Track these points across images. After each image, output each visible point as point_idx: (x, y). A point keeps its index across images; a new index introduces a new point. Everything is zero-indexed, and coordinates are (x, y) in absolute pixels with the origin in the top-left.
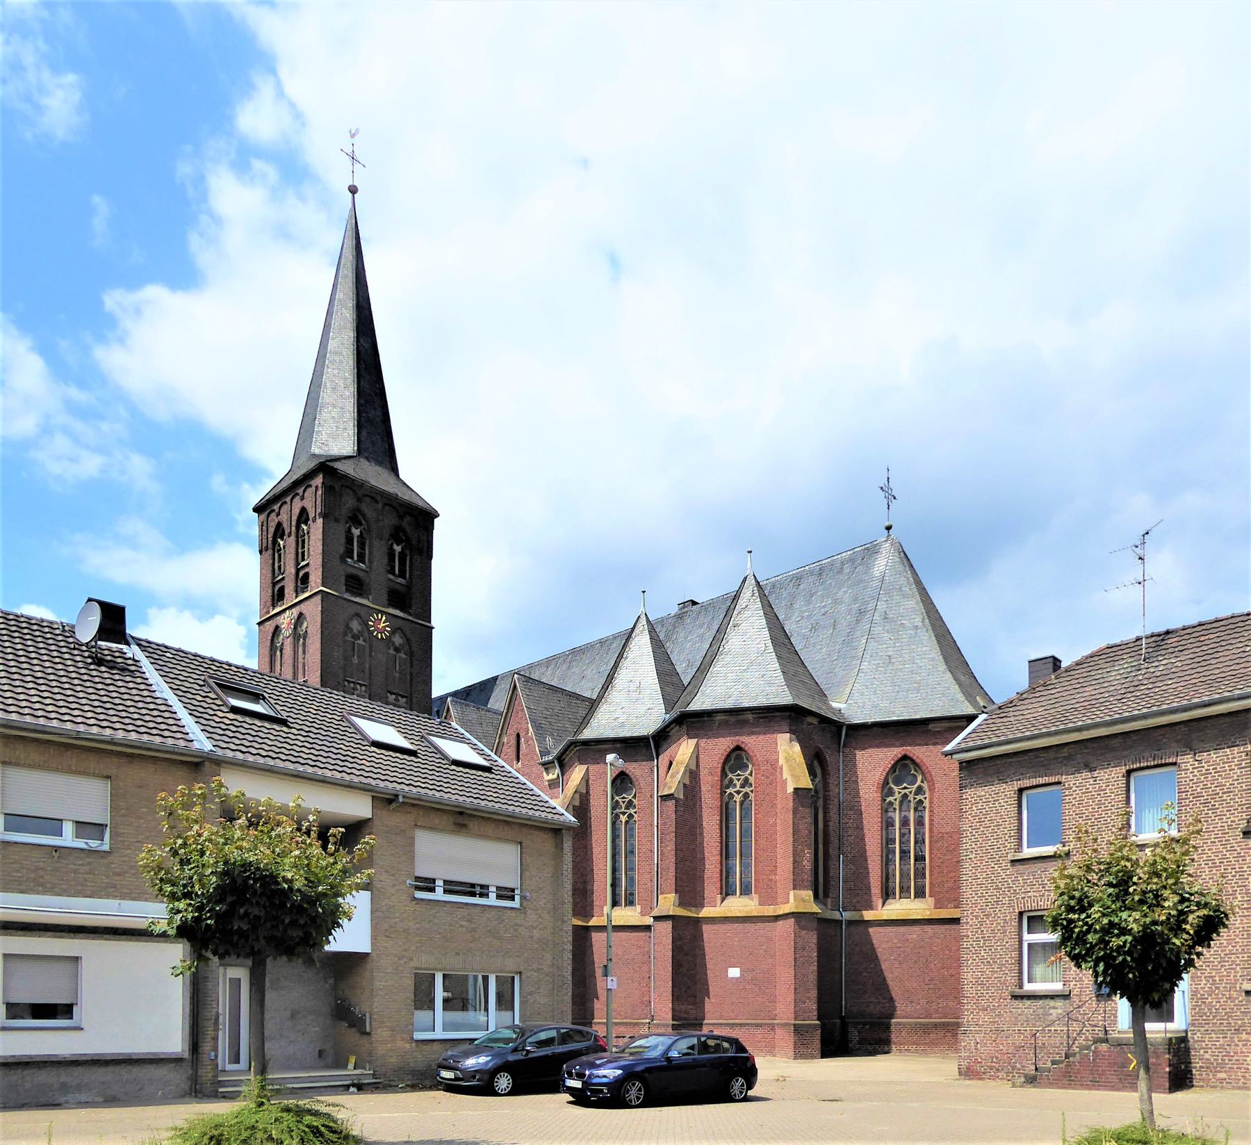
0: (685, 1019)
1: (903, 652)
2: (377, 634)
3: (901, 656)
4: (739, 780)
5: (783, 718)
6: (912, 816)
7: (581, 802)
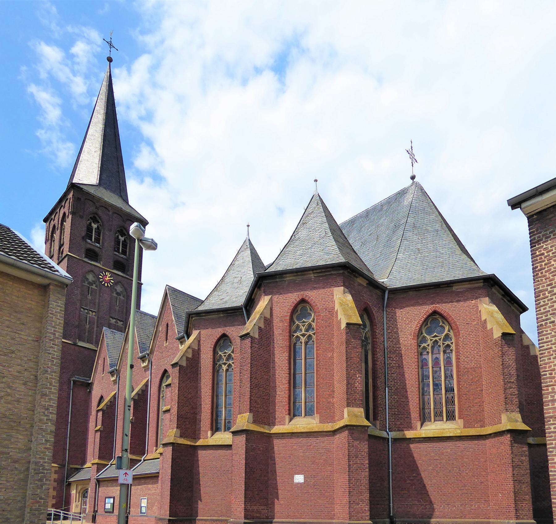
0: (257, 517)
1: (428, 246)
2: (105, 283)
3: (427, 248)
4: (304, 326)
5: (339, 275)
6: (442, 357)
7: (193, 355)
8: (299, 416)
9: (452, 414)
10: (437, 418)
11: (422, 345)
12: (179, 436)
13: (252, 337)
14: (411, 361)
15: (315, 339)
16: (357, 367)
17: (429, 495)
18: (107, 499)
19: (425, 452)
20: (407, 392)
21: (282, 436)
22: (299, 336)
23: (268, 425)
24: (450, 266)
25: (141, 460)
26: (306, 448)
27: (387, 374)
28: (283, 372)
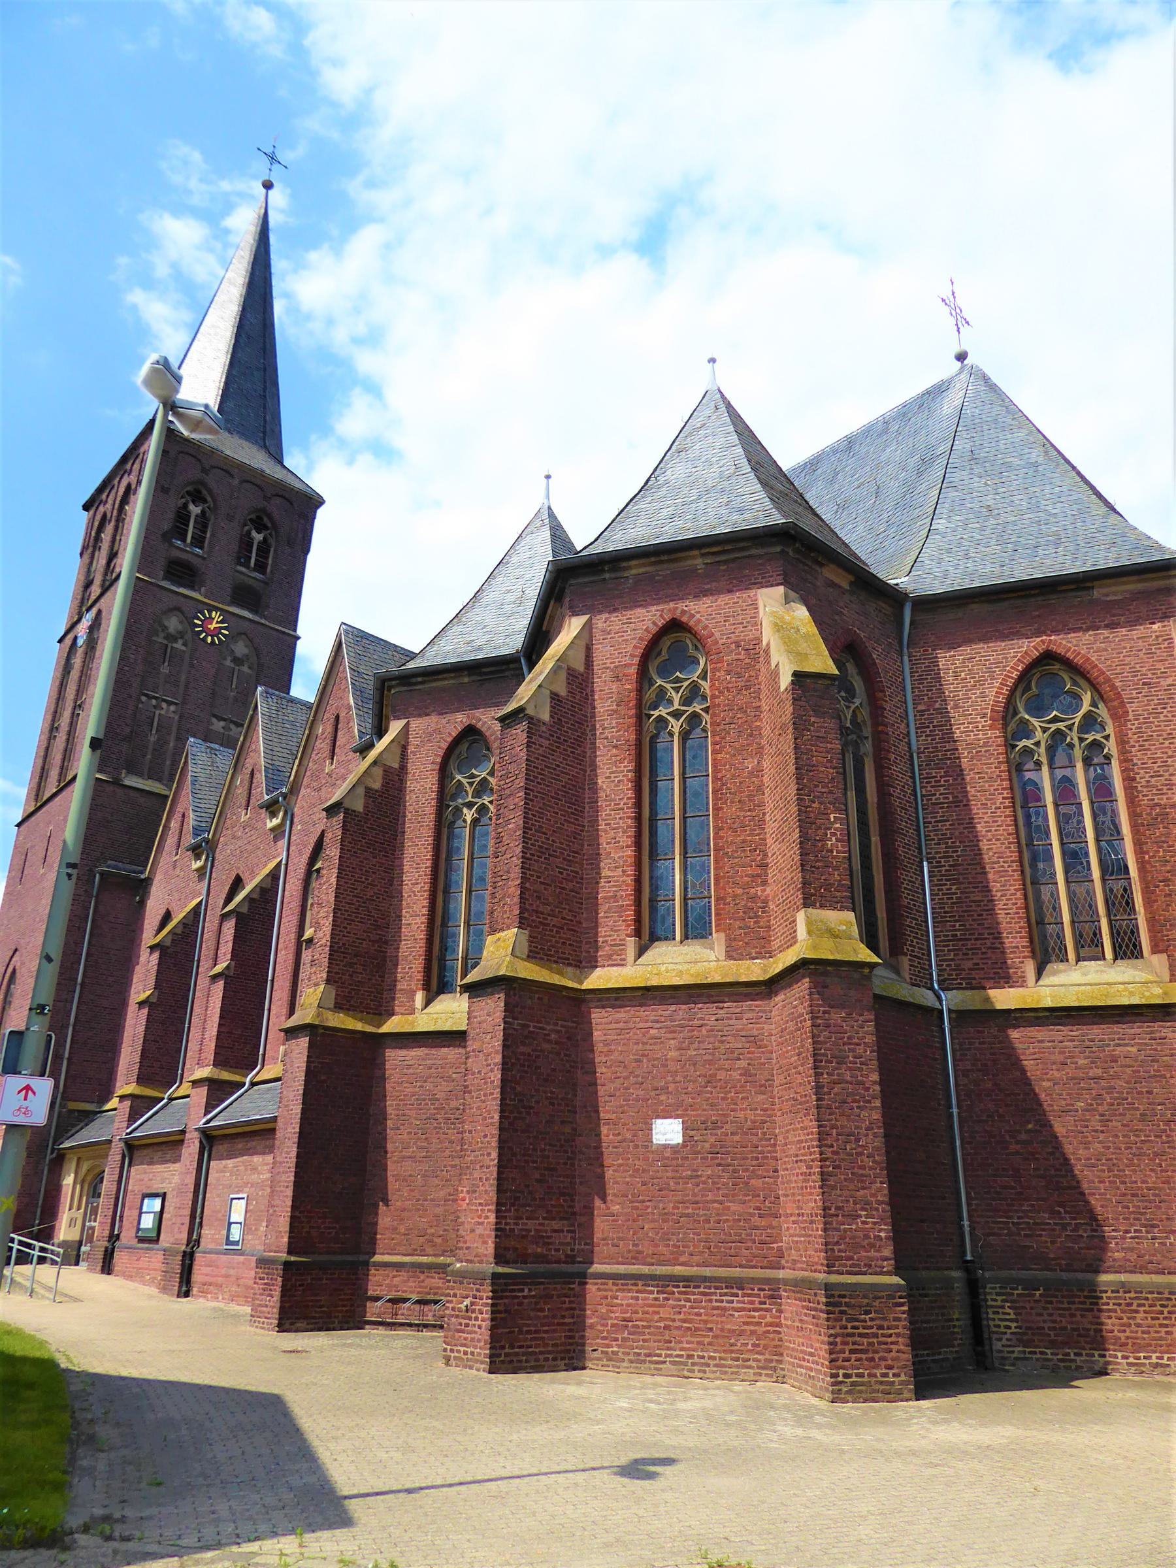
4: (677, 690)
7: (386, 783)
8: (666, 939)
9: (1130, 940)
10: (1083, 952)
11: (1021, 744)
12: (332, 1006)
13: (531, 719)
14: (989, 786)
15: (709, 723)
16: (831, 792)
17: (1083, 1194)
18: (146, 1201)
19: (1060, 1053)
20: (985, 873)
21: (617, 999)
22: (666, 716)
23: (576, 966)
24: (1079, 542)
25: (244, 1084)
26: (686, 1033)
27: (924, 823)
28: (619, 814)
